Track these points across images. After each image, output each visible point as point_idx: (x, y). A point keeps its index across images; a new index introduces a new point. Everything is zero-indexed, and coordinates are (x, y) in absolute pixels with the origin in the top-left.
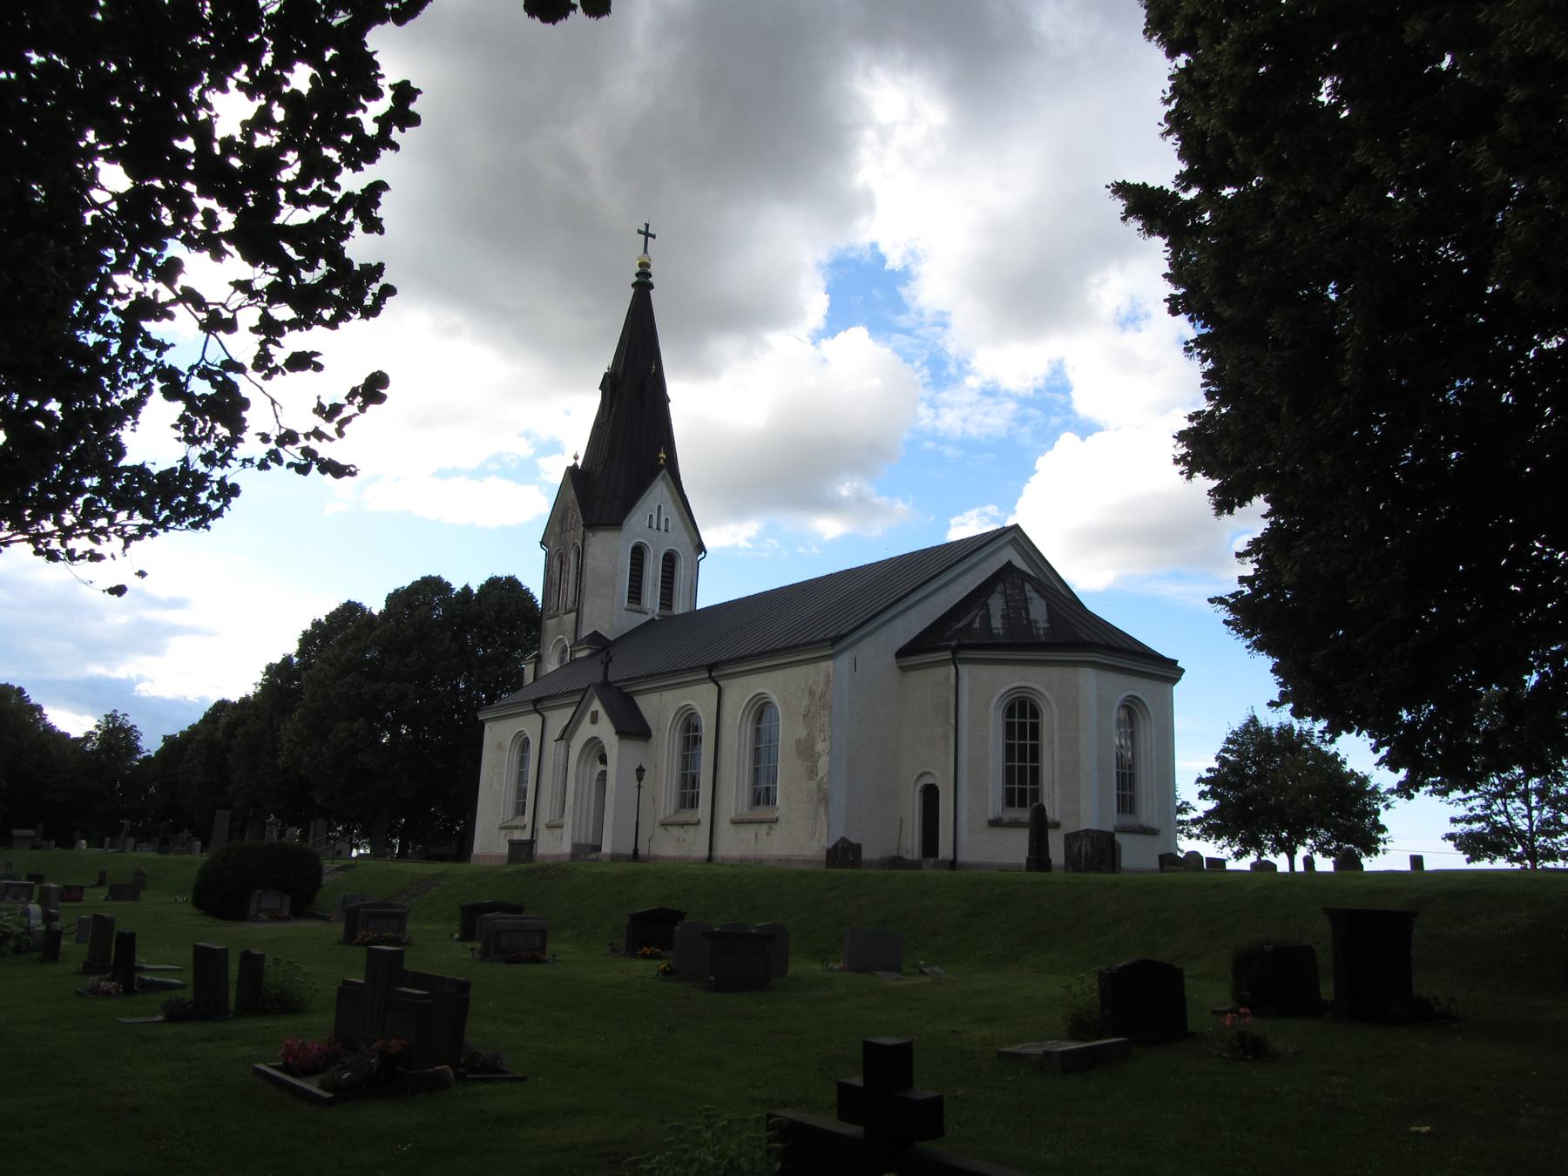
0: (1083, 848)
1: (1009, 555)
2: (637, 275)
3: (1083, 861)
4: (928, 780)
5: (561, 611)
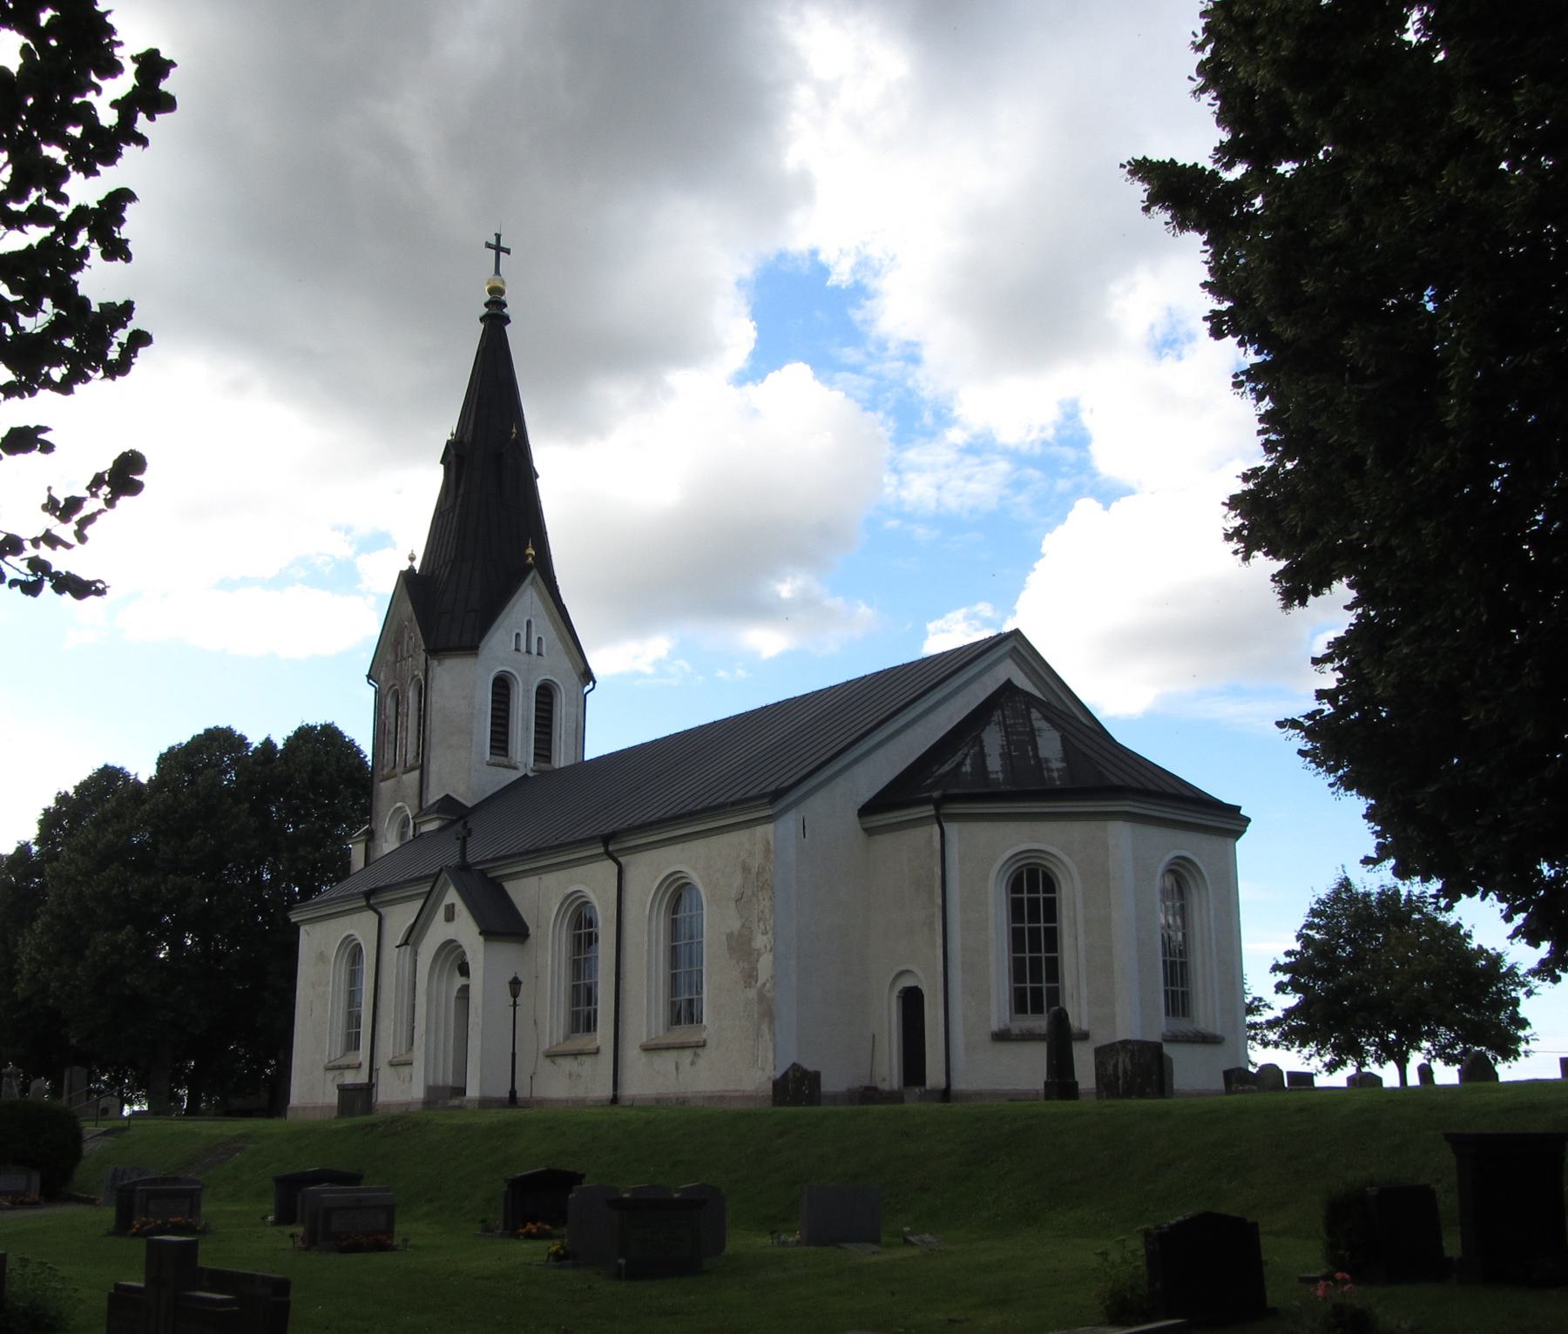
1: (1008, 671)
2: (487, 305)
4: (908, 982)
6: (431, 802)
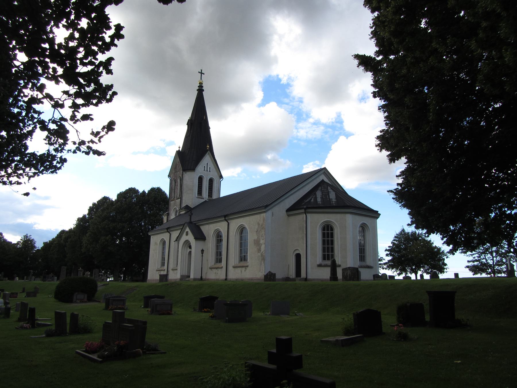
0: (348, 273)
1: (323, 177)
3: (348, 277)
4: (297, 252)
5: (175, 198)
6: (183, 207)
